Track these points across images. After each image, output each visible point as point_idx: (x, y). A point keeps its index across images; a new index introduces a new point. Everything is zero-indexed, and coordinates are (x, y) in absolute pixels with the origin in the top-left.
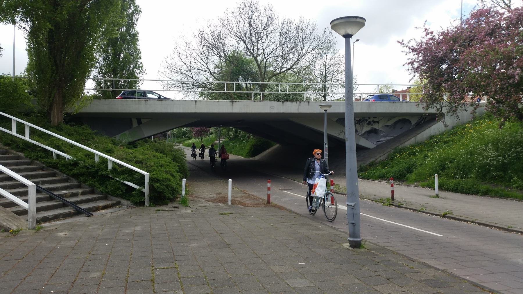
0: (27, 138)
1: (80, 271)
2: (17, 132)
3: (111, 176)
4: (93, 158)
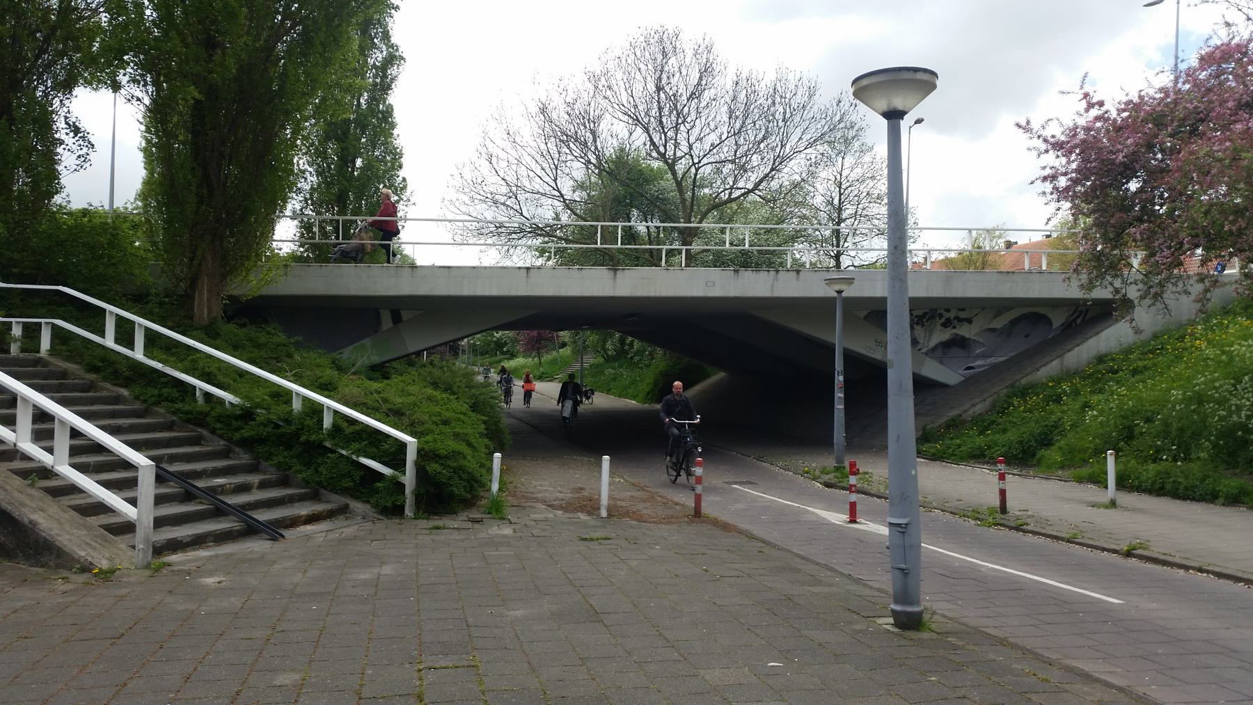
0: (138, 354)
2: (117, 341)
3: (328, 444)
4: (289, 402)
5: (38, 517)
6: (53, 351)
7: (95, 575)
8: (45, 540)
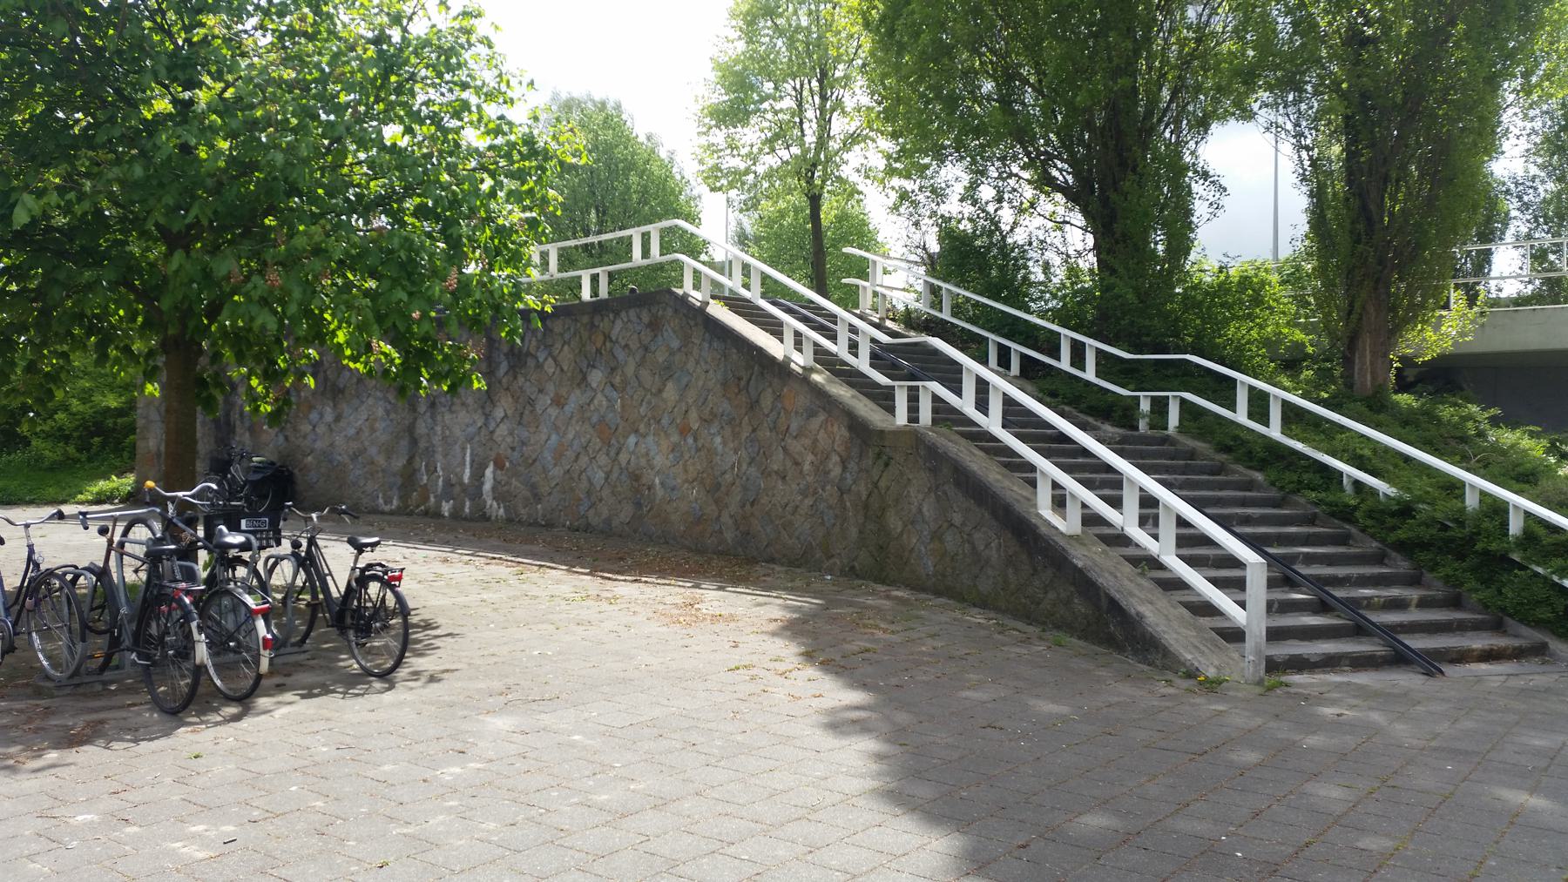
0: (1275, 432)
1: (1335, 822)
2: (1251, 416)
3: (1516, 557)
4: (1462, 497)
5: (1145, 610)
6: (1181, 428)
7: (1200, 683)
8: (1152, 636)
